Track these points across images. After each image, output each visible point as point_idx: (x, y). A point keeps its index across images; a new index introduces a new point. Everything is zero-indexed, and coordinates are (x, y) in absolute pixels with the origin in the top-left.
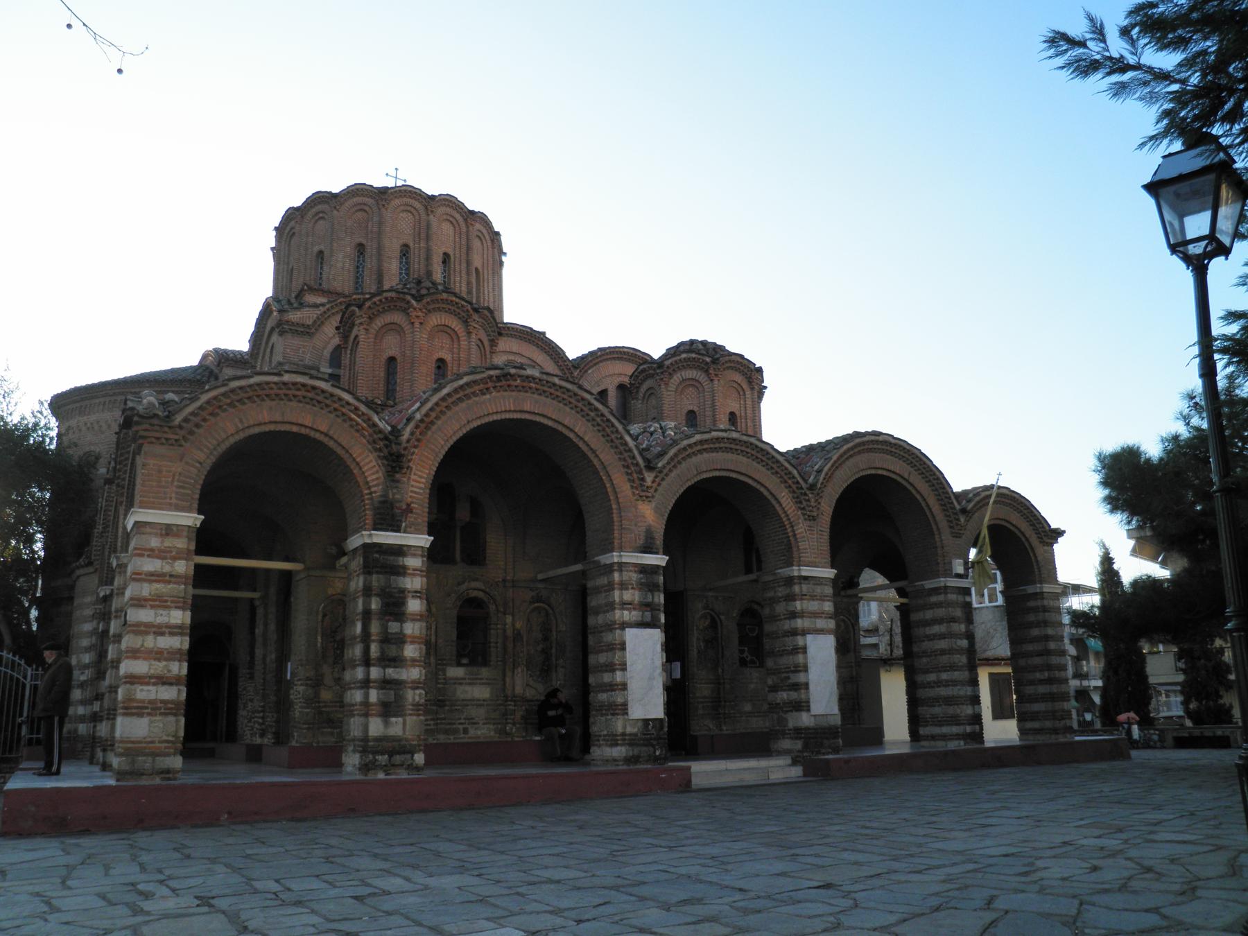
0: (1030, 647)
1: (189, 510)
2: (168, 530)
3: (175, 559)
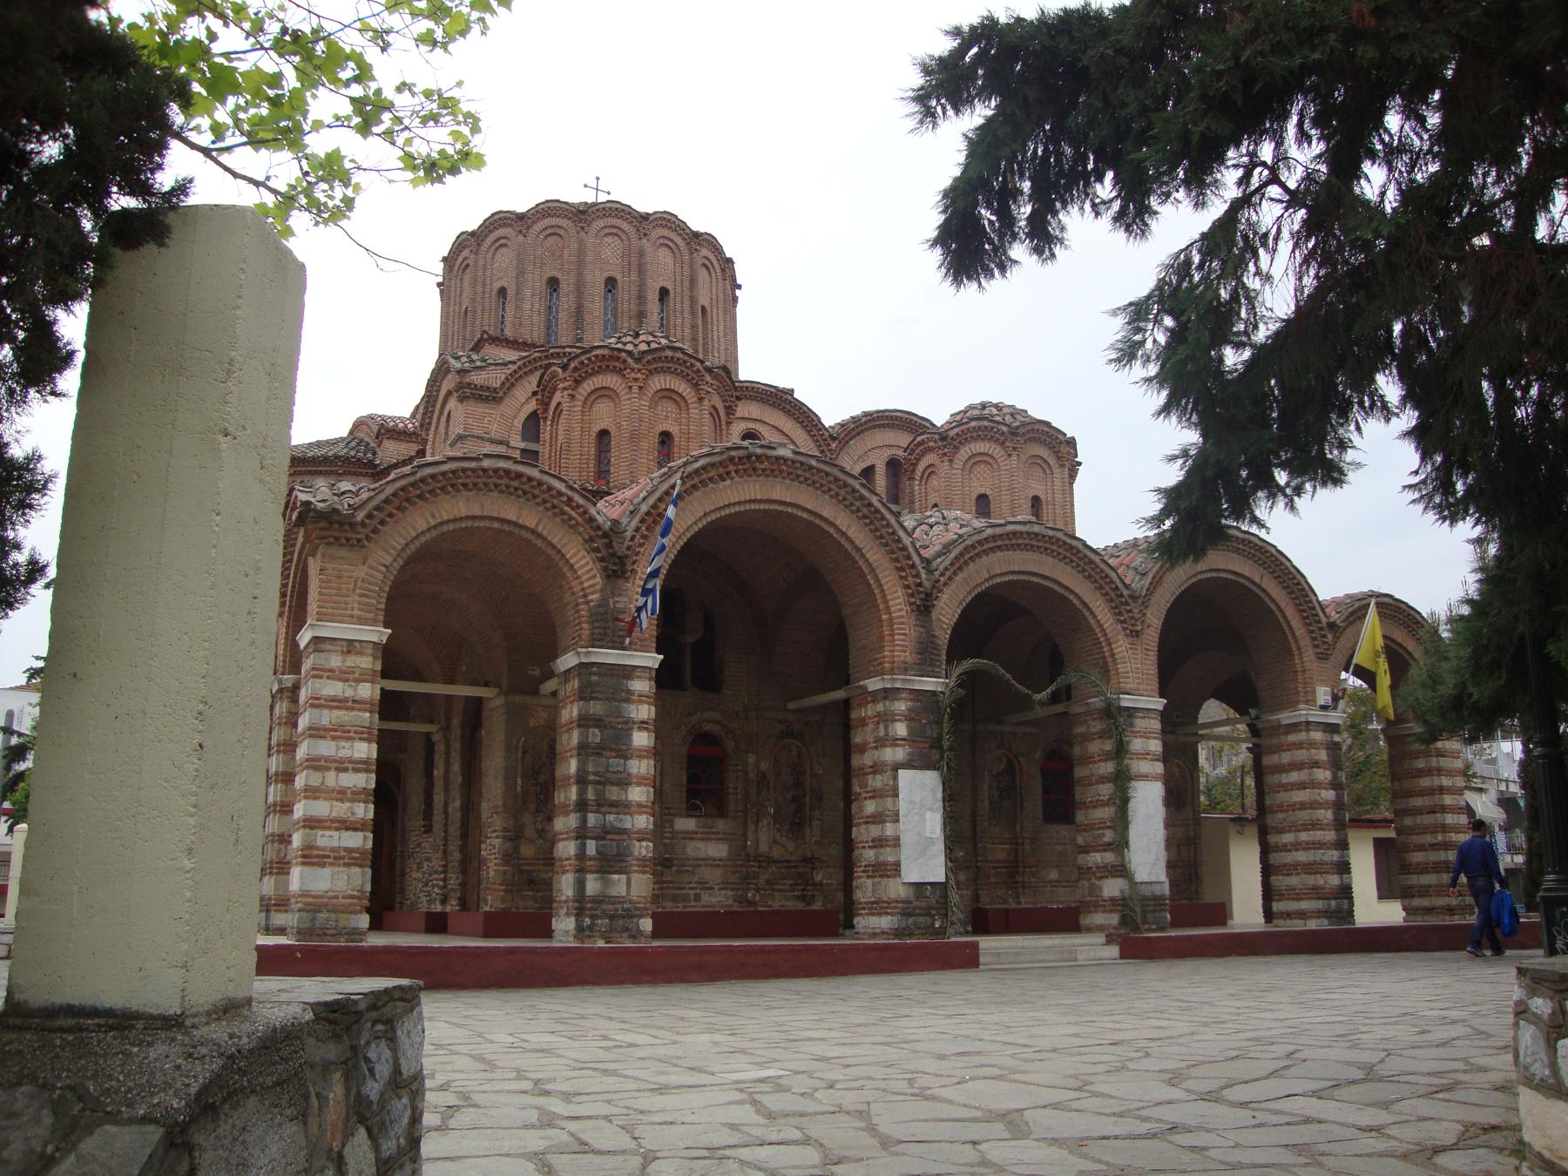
0: (1418, 802)
1: (374, 622)
2: (350, 647)
3: (358, 681)
